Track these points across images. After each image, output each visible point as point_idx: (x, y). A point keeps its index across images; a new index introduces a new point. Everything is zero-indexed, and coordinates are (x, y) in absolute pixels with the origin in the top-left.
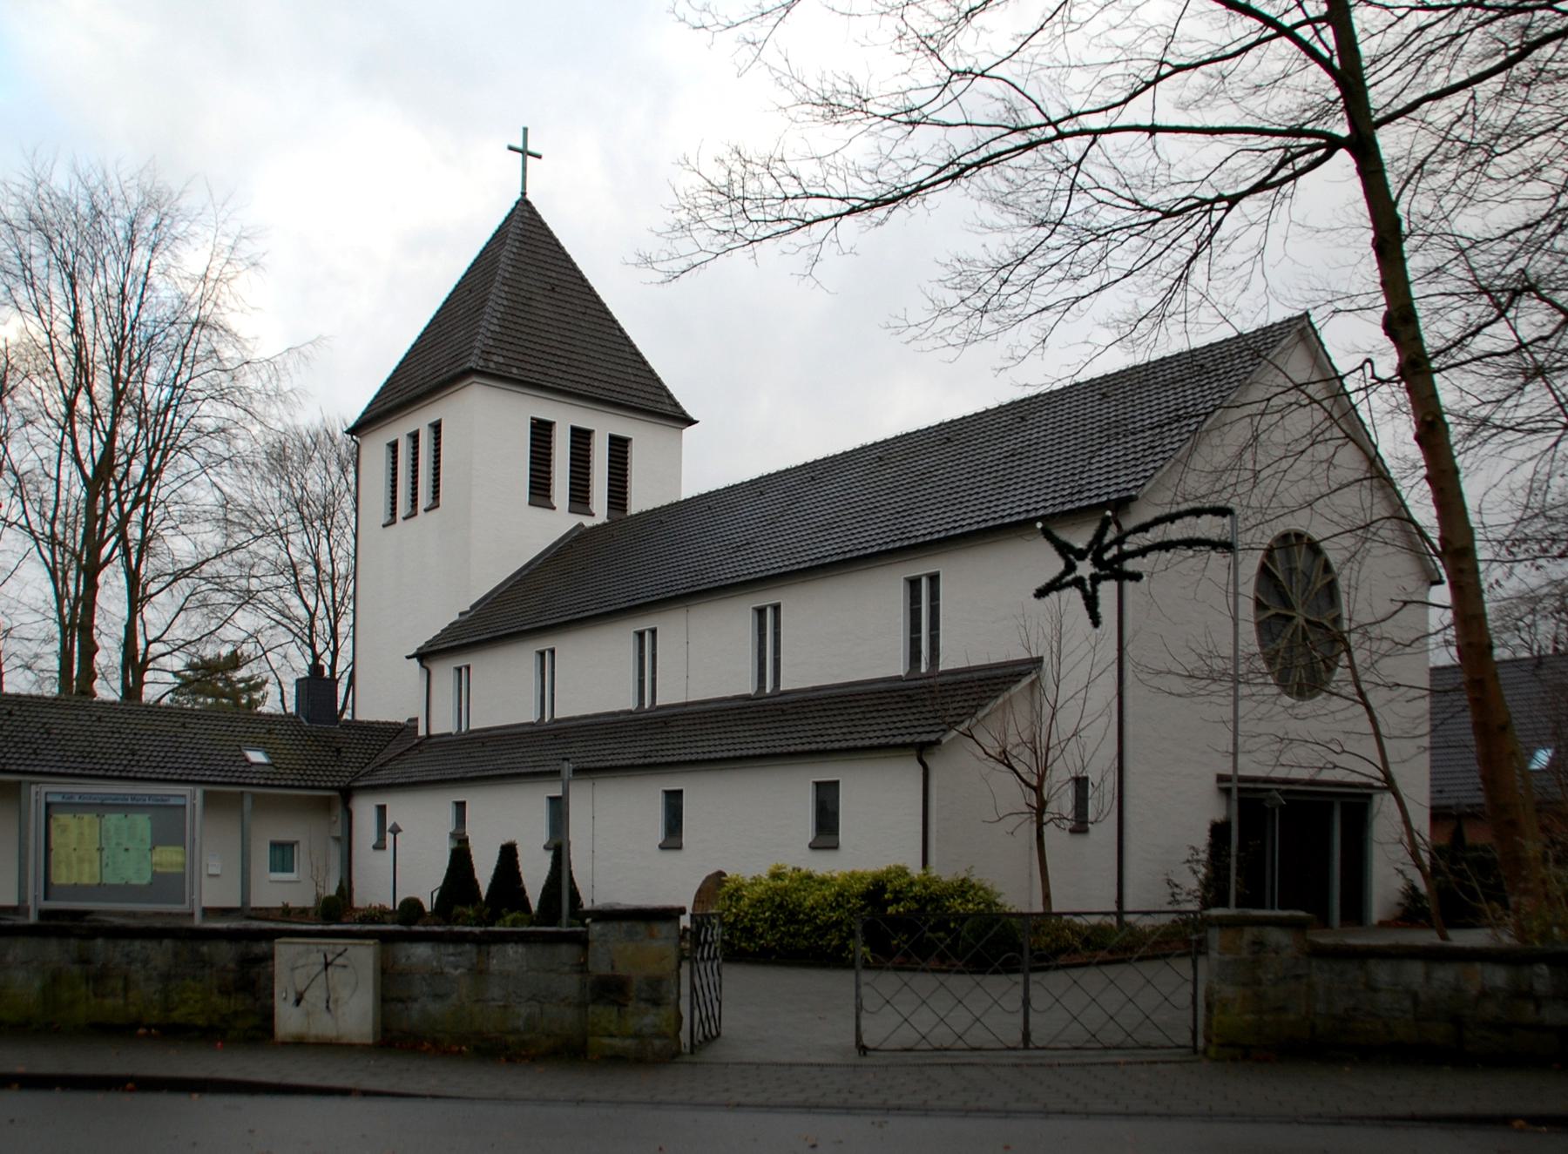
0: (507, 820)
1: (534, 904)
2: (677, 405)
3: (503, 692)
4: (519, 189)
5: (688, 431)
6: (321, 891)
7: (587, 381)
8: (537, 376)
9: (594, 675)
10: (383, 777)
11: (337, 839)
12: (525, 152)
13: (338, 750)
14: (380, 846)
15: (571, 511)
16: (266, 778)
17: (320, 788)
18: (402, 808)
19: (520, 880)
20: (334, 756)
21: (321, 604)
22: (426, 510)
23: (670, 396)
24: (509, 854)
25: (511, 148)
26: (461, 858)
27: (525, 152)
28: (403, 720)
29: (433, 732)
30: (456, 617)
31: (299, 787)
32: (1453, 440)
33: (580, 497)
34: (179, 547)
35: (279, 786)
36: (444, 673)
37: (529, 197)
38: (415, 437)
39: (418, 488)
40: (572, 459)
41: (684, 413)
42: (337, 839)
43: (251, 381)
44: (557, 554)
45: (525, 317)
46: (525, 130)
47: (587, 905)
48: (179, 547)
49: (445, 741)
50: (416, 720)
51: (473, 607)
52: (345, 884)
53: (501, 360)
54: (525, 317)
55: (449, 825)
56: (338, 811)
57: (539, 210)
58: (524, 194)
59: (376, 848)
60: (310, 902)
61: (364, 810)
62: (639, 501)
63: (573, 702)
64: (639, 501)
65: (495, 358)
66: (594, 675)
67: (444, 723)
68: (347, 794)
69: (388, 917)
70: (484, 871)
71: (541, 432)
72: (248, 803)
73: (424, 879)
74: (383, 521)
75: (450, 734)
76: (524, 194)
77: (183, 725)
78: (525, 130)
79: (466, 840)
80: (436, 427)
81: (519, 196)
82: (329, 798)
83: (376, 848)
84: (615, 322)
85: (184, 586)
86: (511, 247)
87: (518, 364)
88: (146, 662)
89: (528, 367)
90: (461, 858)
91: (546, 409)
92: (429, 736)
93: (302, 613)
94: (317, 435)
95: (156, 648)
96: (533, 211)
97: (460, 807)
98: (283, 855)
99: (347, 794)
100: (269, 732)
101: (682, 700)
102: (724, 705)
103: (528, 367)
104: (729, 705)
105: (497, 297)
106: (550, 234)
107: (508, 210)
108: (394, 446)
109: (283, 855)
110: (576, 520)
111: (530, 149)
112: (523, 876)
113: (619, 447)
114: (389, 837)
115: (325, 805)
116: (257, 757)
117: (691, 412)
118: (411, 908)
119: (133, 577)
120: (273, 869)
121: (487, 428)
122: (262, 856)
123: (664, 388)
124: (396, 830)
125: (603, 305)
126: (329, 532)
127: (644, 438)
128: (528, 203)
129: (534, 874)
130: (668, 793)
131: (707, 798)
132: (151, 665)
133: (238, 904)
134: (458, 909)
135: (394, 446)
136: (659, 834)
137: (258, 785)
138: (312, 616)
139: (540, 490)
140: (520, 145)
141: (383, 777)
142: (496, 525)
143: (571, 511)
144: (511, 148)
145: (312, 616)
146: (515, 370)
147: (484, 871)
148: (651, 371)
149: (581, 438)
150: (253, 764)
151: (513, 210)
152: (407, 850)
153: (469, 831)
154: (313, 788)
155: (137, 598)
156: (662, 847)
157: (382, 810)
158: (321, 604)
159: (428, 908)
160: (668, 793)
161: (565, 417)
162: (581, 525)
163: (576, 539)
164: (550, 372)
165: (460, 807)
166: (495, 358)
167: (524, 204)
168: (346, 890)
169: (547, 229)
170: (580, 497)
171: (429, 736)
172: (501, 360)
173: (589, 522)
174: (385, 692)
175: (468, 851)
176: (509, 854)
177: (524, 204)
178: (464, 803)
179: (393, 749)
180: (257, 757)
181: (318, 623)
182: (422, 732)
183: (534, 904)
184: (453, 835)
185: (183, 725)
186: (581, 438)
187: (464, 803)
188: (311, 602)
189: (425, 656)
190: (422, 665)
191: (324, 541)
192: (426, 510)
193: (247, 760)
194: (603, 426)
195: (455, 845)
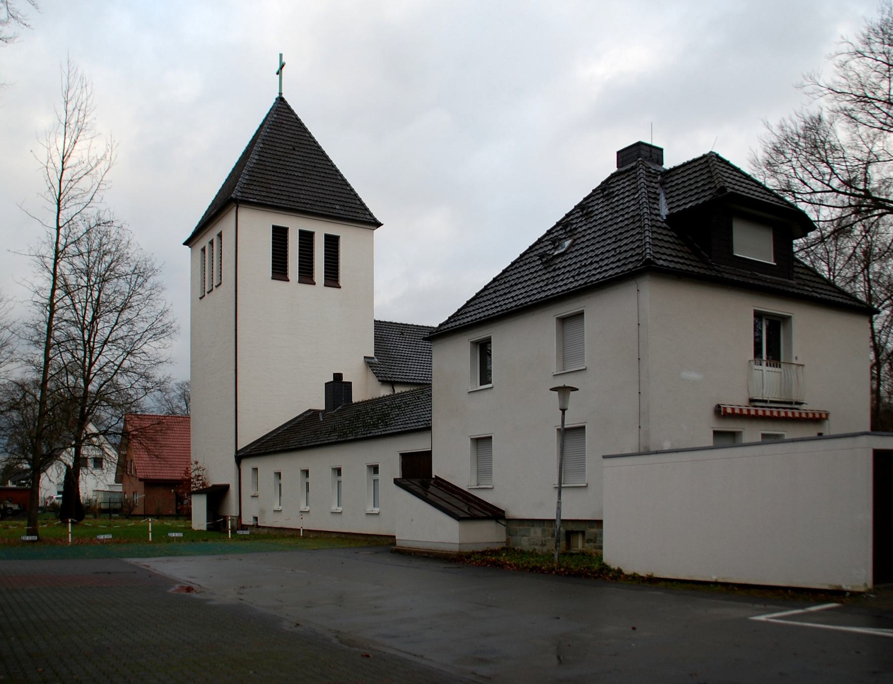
2: (371, 215)
5: (378, 231)
32: (795, 249)
37: (283, 96)
38: (211, 243)
40: (273, 239)
41: (375, 219)
46: (604, 457)
54: (287, 179)
58: (281, 94)
71: (280, 234)
76: (281, 94)
78: (604, 457)
80: (220, 235)
91: (282, 220)
105: (254, 157)
108: (203, 250)
113: (332, 243)
130: (475, 344)
149: (306, 238)
160: (475, 344)
161: (295, 225)
167: (281, 108)
177: (281, 108)
186: (306, 238)
194: (321, 229)
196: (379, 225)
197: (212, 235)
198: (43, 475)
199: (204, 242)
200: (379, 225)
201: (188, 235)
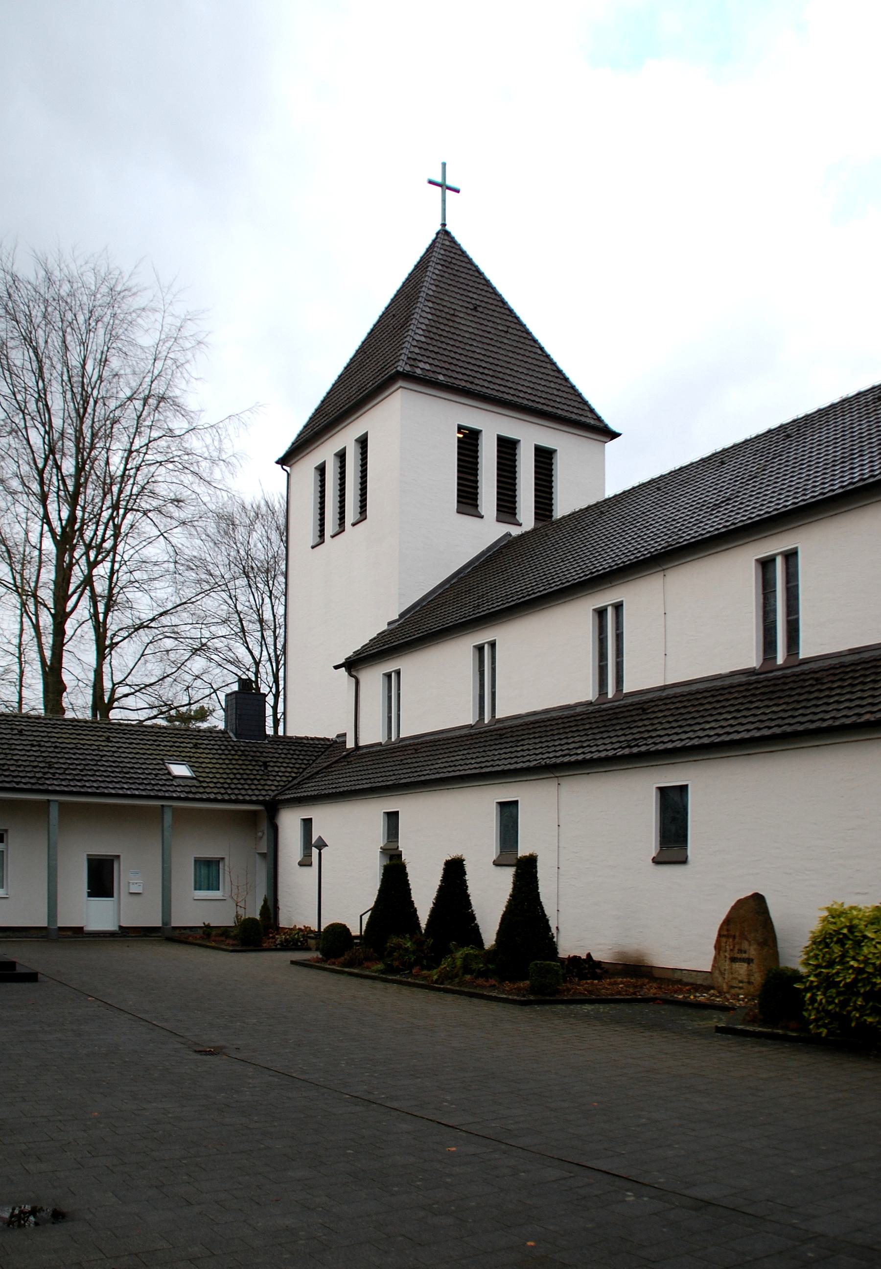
0: (447, 830)
1: (489, 934)
2: (599, 419)
3: (438, 693)
4: (440, 222)
6: (241, 912)
7: (512, 392)
8: (463, 384)
9: (545, 663)
10: (310, 789)
11: (263, 855)
12: (443, 186)
13: (266, 765)
14: (305, 863)
15: (498, 520)
16: (189, 790)
17: (244, 802)
18: (328, 820)
19: (469, 905)
20: (256, 769)
21: (265, 653)
22: (354, 525)
23: (592, 411)
24: (454, 871)
25: (431, 182)
26: (395, 875)
27: (443, 186)
28: (332, 736)
29: (361, 744)
30: (385, 627)
31: (223, 801)
33: (507, 507)
34: (142, 604)
35: (201, 800)
36: (373, 679)
37: (448, 228)
38: (341, 456)
39: (343, 501)
41: (606, 426)
42: (263, 855)
43: (194, 443)
44: (487, 561)
45: (449, 333)
46: (444, 165)
47: (569, 944)
48: (142, 604)
49: (376, 752)
50: (345, 735)
51: (402, 616)
52: (270, 904)
53: (427, 367)
54: (449, 333)
55: (378, 837)
56: (264, 826)
57: (459, 239)
58: (444, 225)
59: (301, 864)
60: (228, 921)
61: (290, 823)
62: (564, 504)
63: (515, 700)
64: (564, 504)
65: (422, 365)
66: (545, 663)
67: (373, 733)
68: (272, 809)
69: (312, 942)
70: (424, 895)
71: (469, 441)
72: (168, 817)
73: (350, 901)
74: (312, 544)
75: (380, 744)
76: (444, 225)
77: (108, 739)
78: (444, 165)
79: (400, 856)
80: (363, 442)
81: (439, 228)
82: (255, 812)
83: (301, 864)
84: (535, 341)
85: (144, 636)
86: (433, 269)
87: (445, 372)
88: (112, 700)
89: (455, 375)
90: (395, 875)
92: (357, 747)
93: (248, 660)
94: (259, 507)
95: (121, 691)
96: (453, 240)
97: (392, 818)
98: (208, 872)
99: (273, 808)
100: (196, 746)
101: (660, 683)
102: (718, 683)
103: (455, 375)
104: (727, 682)
105: (433, 269)
106: (470, 261)
107: (429, 242)
108: (321, 470)
109: (208, 872)
110: (503, 529)
111: (449, 183)
112: (472, 899)
113: (545, 458)
114: (315, 851)
115: (250, 821)
116: (180, 770)
117: (614, 426)
118: (339, 931)
119: (100, 630)
120: (198, 887)
121: (413, 433)
122: (185, 873)
123: (585, 403)
124: (321, 845)
125: (523, 326)
126: (271, 592)
127: (567, 446)
128: (447, 233)
129: (490, 896)
131: (717, 792)
132: (116, 704)
133: (159, 924)
134: (394, 941)
135: (321, 470)
136: (651, 844)
137: (179, 799)
138: (257, 664)
139: (468, 499)
140: (439, 179)
141: (310, 789)
142: (420, 529)
143: (498, 520)
144: (431, 182)
145: (257, 664)
146: (441, 377)
147: (424, 895)
148: (573, 387)
149: (507, 448)
150: (175, 777)
151: (434, 241)
152: (333, 866)
153: (404, 845)
154: (237, 801)
155: (103, 648)
156: (657, 861)
157: (307, 823)
158: (265, 653)
159: (355, 931)
161: (492, 426)
162: (508, 534)
163: (504, 546)
164: (476, 381)
165: (392, 818)
166: (422, 365)
167: (444, 234)
168: (271, 908)
169: (467, 257)
170: (507, 507)
171: (357, 747)
172: (427, 367)
173: (515, 531)
174: (316, 707)
175: (403, 867)
176: (454, 871)
177: (444, 234)
178: (396, 813)
179: (323, 762)
180: (180, 770)
181: (262, 670)
182: (350, 744)
183: (489, 934)
184: (384, 850)
185: (108, 739)
186: (507, 448)
187: (396, 813)
188: (257, 654)
189: (353, 665)
190: (350, 675)
191: (267, 600)
192: (354, 525)
193: (169, 773)
194: (530, 436)
195: (386, 862)
196: (614, 435)
197: (345, 438)
198: (95, 666)
199: (325, 453)
200: (614, 435)
201: (281, 453)
